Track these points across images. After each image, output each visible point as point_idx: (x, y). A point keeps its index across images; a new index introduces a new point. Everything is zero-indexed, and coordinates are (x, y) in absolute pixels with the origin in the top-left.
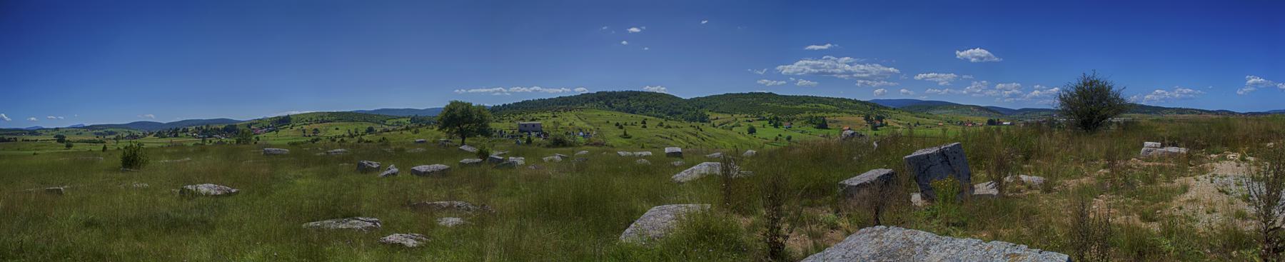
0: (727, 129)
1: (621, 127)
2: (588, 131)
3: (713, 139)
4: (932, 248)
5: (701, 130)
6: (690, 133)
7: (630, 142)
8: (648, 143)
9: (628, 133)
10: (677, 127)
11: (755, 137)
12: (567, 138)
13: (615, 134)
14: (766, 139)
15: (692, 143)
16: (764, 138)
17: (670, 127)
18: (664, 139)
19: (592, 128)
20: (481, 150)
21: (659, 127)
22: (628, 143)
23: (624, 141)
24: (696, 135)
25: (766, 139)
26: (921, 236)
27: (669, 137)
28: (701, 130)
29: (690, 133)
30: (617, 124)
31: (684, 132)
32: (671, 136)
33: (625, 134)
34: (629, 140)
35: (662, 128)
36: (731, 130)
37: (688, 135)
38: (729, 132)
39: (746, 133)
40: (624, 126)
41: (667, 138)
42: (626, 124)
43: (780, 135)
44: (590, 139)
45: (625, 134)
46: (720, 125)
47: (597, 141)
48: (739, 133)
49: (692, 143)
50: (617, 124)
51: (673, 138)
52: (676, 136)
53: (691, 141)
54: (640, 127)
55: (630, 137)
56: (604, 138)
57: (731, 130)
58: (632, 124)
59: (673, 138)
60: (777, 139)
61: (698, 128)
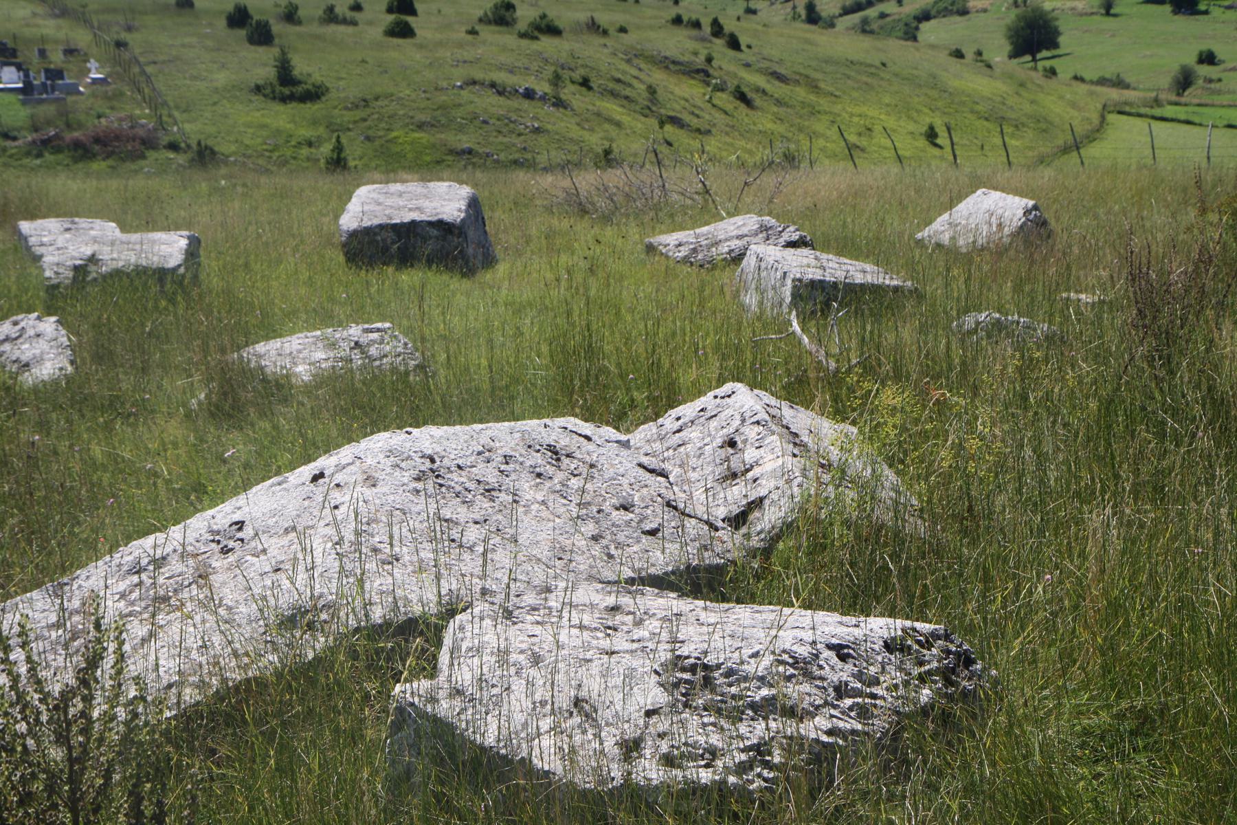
0: (887, 32)
1: (262, 36)
2: (57, 58)
3: (801, 93)
4: (215, 528)
5: (734, 44)
6: (668, 64)
7: (314, 123)
8: (421, 126)
9: (300, 66)
10: (594, 27)
11: (1052, 72)
12: (534, 136)
13: (222, 78)
14: (1119, 83)
15: (675, 121)
16: (1102, 82)
17: (553, 30)
18: (515, 103)
19: (81, 37)
20: (93, 255)
21: (487, 33)
22: (306, 133)
23: (282, 117)
24: (702, 73)
25: (1119, 83)
26: (287, 475)
27: (543, 88)
28: (734, 44)
29: (668, 64)
30: (239, 18)
31: (635, 55)
32: (556, 80)
33: (285, 75)
34: (310, 109)
35: (508, 39)
36: (911, 35)
37: (658, 77)
38: (895, 50)
39: (999, 50)
40: (277, 28)
41: (529, 94)
42: (291, 16)
43: (1208, 58)
44: (64, 114)
45: (285, 75)
46: (847, 11)
47: (111, 121)
48: (959, 54)
49: (675, 121)
50: (239, 18)
51: (569, 92)
52: (585, 83)
53: (674, 109)
54: (376, 33)
55: (313, 95)
56: (155, 103)
57: (911, 35)
58: (331, 16)
59: (569, 92)
60: (1185, 81)
61: (717, 29)
